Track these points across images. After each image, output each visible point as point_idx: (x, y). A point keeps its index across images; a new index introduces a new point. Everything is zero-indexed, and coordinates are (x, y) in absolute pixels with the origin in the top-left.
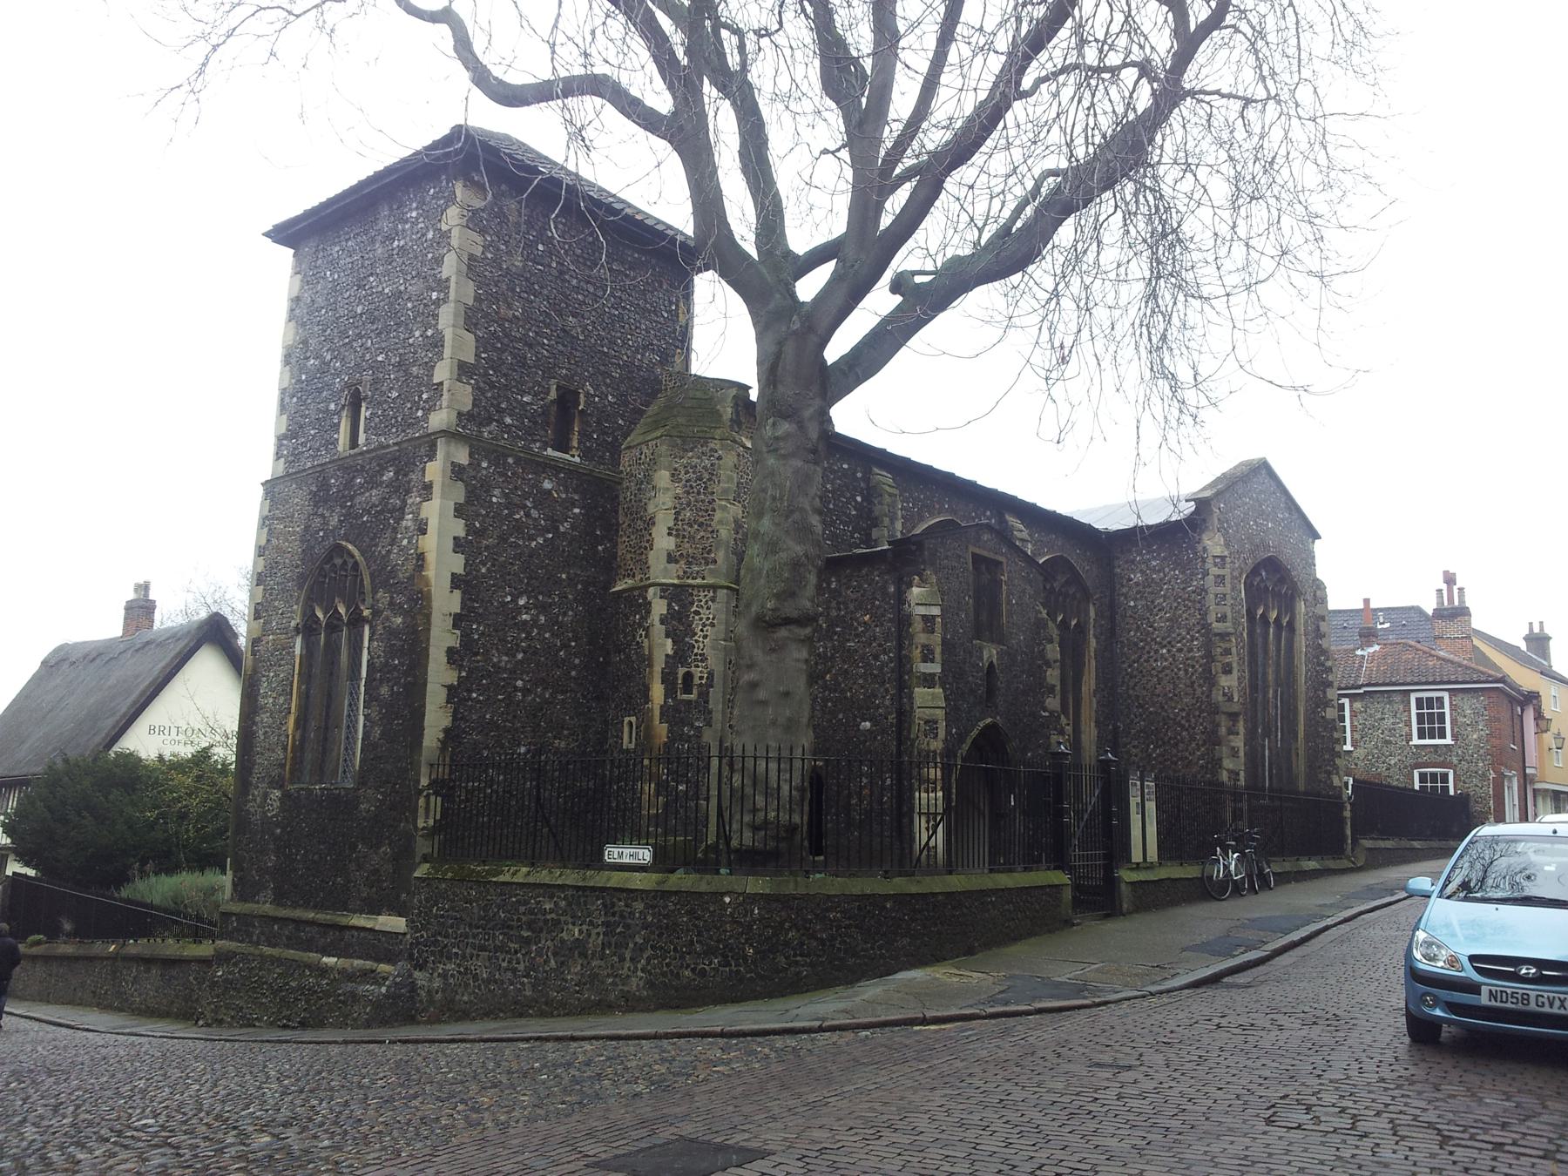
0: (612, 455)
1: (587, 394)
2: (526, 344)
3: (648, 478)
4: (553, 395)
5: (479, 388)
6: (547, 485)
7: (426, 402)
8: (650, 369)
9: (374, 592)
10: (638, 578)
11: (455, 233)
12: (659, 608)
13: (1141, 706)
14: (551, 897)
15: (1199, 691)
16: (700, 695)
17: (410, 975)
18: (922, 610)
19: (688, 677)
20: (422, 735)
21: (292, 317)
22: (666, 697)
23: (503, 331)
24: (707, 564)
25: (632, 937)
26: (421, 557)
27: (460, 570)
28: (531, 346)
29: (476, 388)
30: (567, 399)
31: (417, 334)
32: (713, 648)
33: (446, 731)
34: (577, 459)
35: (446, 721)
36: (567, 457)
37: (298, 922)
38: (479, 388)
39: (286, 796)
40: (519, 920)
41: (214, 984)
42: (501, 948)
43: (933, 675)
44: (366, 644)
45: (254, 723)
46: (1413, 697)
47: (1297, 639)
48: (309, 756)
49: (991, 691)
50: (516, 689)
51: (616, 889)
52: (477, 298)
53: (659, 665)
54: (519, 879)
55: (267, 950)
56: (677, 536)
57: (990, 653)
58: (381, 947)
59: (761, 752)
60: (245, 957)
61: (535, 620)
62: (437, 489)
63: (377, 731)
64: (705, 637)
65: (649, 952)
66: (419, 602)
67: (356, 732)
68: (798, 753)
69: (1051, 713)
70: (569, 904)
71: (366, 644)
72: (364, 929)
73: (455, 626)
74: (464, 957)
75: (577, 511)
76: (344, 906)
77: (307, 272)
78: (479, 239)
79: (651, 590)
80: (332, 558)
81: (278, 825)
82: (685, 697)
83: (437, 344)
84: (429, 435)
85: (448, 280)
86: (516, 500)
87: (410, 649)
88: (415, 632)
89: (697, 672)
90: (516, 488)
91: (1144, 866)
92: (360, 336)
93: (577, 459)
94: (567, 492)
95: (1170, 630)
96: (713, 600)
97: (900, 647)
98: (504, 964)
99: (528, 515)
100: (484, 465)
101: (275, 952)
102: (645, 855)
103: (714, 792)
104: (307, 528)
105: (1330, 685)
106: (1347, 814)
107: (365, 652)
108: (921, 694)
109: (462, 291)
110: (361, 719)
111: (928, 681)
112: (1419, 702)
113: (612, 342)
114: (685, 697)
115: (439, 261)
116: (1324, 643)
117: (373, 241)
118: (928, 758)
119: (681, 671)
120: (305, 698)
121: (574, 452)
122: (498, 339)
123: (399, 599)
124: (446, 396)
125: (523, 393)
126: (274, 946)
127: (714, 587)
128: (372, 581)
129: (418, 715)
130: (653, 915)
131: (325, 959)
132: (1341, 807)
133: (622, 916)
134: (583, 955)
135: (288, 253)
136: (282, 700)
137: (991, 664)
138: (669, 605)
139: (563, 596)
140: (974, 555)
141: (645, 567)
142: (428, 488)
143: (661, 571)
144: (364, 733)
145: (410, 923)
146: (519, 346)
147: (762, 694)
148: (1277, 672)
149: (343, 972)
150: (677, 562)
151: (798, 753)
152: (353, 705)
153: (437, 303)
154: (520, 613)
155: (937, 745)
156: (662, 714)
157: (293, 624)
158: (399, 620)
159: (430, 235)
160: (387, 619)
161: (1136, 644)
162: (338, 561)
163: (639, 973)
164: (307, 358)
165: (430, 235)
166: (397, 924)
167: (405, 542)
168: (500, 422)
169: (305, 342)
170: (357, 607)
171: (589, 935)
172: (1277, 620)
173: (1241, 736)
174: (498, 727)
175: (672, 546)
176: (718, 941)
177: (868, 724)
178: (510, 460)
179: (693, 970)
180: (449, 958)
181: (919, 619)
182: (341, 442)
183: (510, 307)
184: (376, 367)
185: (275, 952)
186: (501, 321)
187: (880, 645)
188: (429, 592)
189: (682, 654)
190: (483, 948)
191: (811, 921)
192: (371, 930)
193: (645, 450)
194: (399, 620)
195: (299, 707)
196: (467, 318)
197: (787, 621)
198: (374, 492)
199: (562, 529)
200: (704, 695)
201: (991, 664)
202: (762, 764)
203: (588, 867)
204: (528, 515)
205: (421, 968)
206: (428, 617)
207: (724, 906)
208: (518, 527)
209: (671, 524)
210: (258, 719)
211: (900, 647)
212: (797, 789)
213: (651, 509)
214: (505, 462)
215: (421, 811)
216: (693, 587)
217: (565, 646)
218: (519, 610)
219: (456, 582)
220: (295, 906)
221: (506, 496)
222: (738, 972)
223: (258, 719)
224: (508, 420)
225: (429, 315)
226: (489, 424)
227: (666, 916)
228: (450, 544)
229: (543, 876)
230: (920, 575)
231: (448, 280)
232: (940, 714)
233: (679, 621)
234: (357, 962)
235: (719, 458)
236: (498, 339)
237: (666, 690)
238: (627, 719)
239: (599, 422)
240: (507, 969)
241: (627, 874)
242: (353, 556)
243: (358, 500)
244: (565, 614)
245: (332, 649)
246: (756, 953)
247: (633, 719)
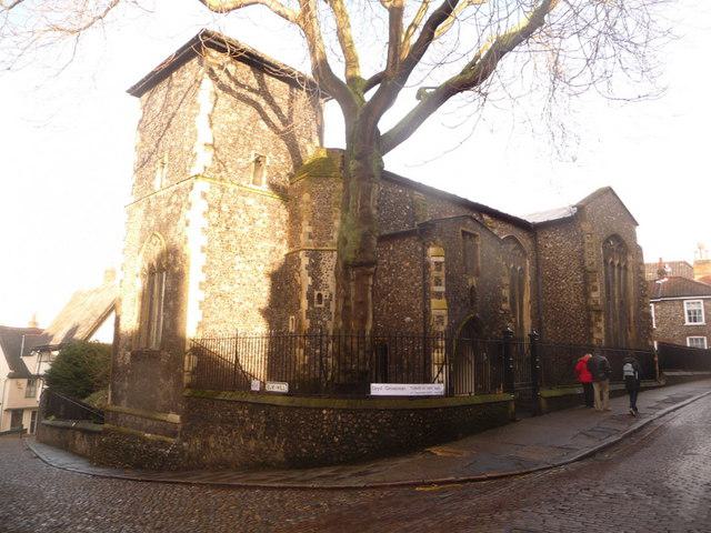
19: (320, 296)
43: (441, 293)
46: (685, 302)
53: (305, 290)
79: (301, 253)
111: (438, 295)
118: (437, 336)
119: (316, 293)
172: (619, 265)
177: (408, 319)
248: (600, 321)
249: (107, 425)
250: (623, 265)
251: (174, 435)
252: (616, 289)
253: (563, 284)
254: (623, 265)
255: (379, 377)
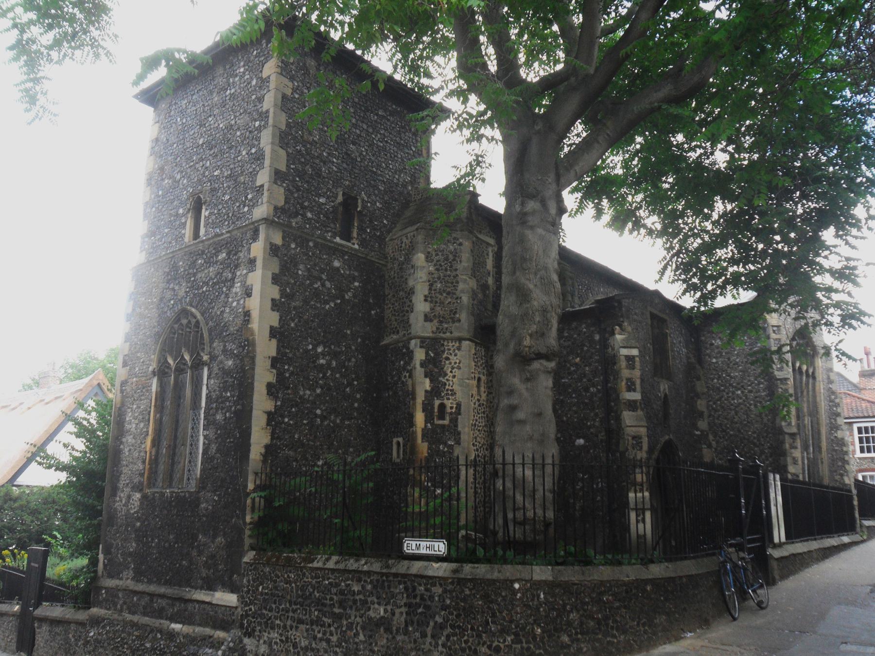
0: (380, 245)
1: (363, 200)
2: (321, 161)
3: (408, 259)
4: (340, 198)
5: (289, 190)
6: (336, 264)
7: (251, 200)
8: (405, 186)
9: (211, 342)
10: (401, 333)
11: (273, 78)
12: (420, 355)
13: (724, 431)
14: (359, 580)
15: (765, 420)
16: (451, 421)
17: (241, 641)
18: (624, 352)
19: (442, 406)
20: (249, 450)
21: (153, 153)
22: (426, 422)
23: (306, 150)
24: (454, 322)
25: (433, 617)
26: (247, 314)
27: (276, 323)
28: (324, 163)
29: (287, 190)
30: (349, 202)
31: (244, 153)
32: (461, 385)
33: (267, 447)
34: (356, 247)
35: (267, 440)
36: (349, 244)
37: (152, 595)
38: (289, 190)
39: (144, 497)
40: (331, 599)
41: (87, 643)
42: (317, 622)
43: (635, 401)
44: (205, 382)
45: (122, 443)
46: (855, 426)
47: (817, 384)
48: (161, 467)
49: (666, 416)
50: (316, 416)
51: (416, 576)
52: (288, 125)
53: (420, 398)
54: (331, 565)
55: (129, 617)
56: (431, 302)
57: (664, 387)
58: (220, 619)
59: (518, 460)
60: (111, 623)
61: (329, 364)
62: (259, 263)
63: (214, 447)
64: (454, 377)
65: (449, 630)
66: (247, 347)
67: (197, 448)
68: (549, 461)
69: (702, 431)
70: (375, 587)
71: (205, 382)
72: (203, 602)
73: (273, 366)
74: (285, 627)
75: (356, 284)
76: (188, 583)
77: (165, 123)
78: (290, 84)
79: (413, 342)
80: (179, 320)
81: (138, 519)
82: (441, 422)
83: (259, 158)
84: (253, 223)
85: (267, 111)
86: (315, 273)
87: (241, 383)
88: (243, 370)
89: (448, 403)
90: (315, 265)
91: (781, 545)
92: (201, 160)
93: (356, 247)
94: (350, 269)
95: (743, 378)
96: (459, 349)
97: (606, 381)
98: (320, 635)
99: (323, 285)
100: (293, 246)
101: (135, 618)
102: (440, 547)
103: (463, 495)
104: (161, 300)
105: (838, 415)
106: (856, 503)
107: (204, 388)
108: (628, 418)
109: (277, 119)
110: (201, 438)
111: (632, 405)
112: (860, 430)
113: (379, 166)
114: (441, 422)
115: (260, 100)
116: (834, 387)
117: (211, 92)
118: (636, 464)
119: (437, 403)
120: (159, 424)
121: (354, 241)
122: (302, 155)
123: (230, 346)
124: (266, 194)
125: (320, 196)
126: (134, 613)
127: (460, 340)
128: (210, 334)
129: (246, 434)
130: (451, 599)
131: (173, 626)
132: (851, 498)
133: (422, 598)
134: (388, 630)
135: (149, 110)
136: (142, 425)
137: (666, 395)
138: (427, 354)
139: (348, 347)
140: (651, 313)
141: (407, 325)
142: (252, 262)
143: (420, 327)
144: (204, 450)
145: (241, 598)
146: (317, 161)
147: (521, 415)
148: (808, 407)
149: (186, 636)
150: (431, 321)
151: (549, 461)
152: (195, 428)
153: (259, 129)
154: (318, 358)
155: (642, 455)
156: (423, 436)
157: (151, 369)
158: (230, 363)
159: (254, 82)
160: (221, 362)
161: (718, 388)
162: (184, 322)
163: (440, 648)
164: (163, 180)
165: (254, 82)
166: (229, 599)
167: (235, 304)
168: (304, 216)
169: (162, 169)
170: (198, 354)
171: (393, 614)
172: (807, 371)
173: (799, 450)
174: (303, 445)
175: (428, 309)
176: (511, 621)
177: (581, 441)
178: (311, 244)
179: (489, 647)
180: (273, 628)
181: (623, 358)
182: (187, 235)
183: (310, 134)
184: (213, 180)
185: (135, 618)
186: (304, 143)
187: (589, 380)
188: (254, 340)
189: (436, 391)
190: (301, 622)
191: (587, 604)
192: (209, 603)
193: (404, 240)
194: (230, 363)
195: (155, 430)
196: (281, 138)
197: (539, 356)
198: (211, 269)
199: (347, 297)
200: (454, 421)
201: (666, 395)
202: (519, 470)
203: (389, 557)
204: (323, 285)
205: (249, 635)
206: (253, 359)
207: (514, 592)
208: (317, 294)
209: (426, 293)
210: (124, 440)
211: (606, 381)
212: (550, 491)
213: (411, 283)
214: (307, 245)
215: (248, 509)
216: (444, 339)
217: (350, 384)
218: (317, 356)
219: (273, 333)
220: (150, 582)
221: (308, 270)
222: (528, 649)
223: (124, 440)
224: (309, 215)
225: (253, 137)
226: (296, 216)
227: (464, 600)
228: (269, 304)
229: (352, 564)
230: (620, 326)
231: (267, 111)
232: (643, 431)
233: (435, 366)
234: (198, 629)
235: (461, 244)
236: (302, 155)
237: (426, 416)
238: (395, 440)
239: (371, 221)
240: (321, 640)
241: (426, 563)
242: (195, 317)
243: (199, 275)
244: (349, 360)
245: (179, 387)
246: (543, 632)
247: (401, 440)
248: (796, 448)
249: (95, 610)
250: (811, 371)
251: (224, 626)
252: (805, 405)
253: (738, 397)
254: (811, 371)
255: (423, 532)
